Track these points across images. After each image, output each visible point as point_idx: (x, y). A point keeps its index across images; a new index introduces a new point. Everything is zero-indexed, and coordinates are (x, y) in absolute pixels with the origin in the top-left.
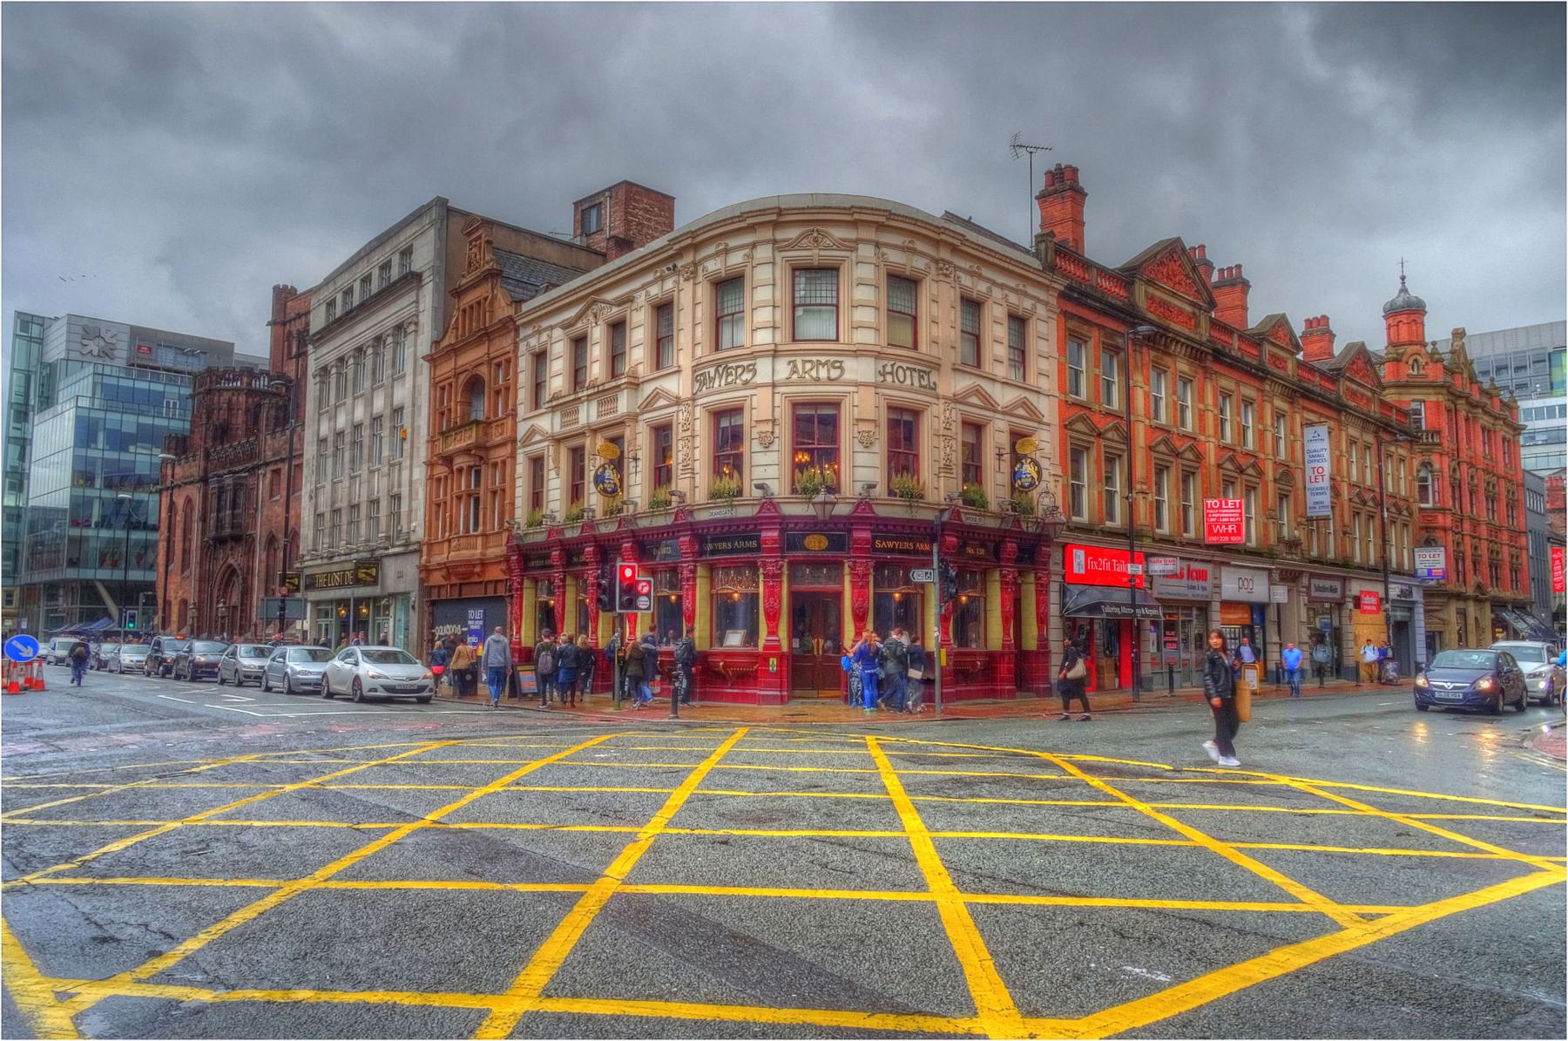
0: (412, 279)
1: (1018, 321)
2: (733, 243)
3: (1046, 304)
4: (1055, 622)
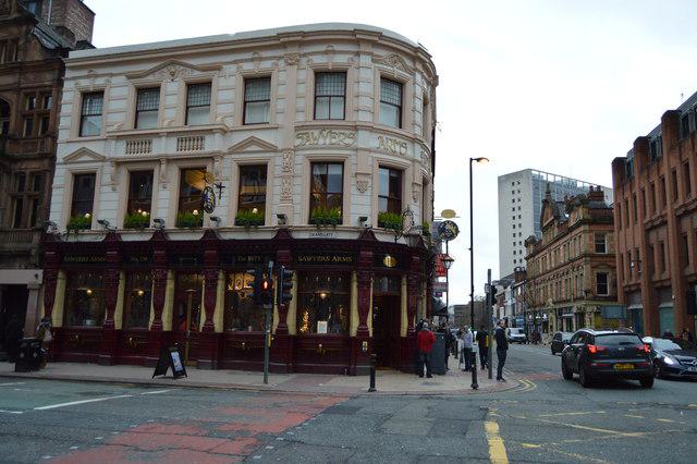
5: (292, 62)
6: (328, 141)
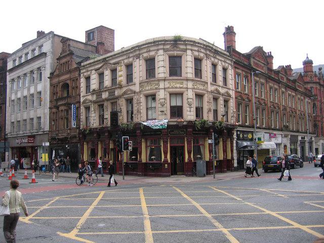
0: (43, 55)
1: (225, 70)
2: (151, 49)
3: (231, 65)
4: (235, 151)
5: (138, 57)
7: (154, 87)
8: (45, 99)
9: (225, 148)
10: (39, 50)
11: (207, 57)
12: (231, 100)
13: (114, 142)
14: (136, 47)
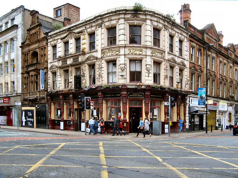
0: (15, 27)
1: (181, 42)
2: (113, 18)
3: (187, 38)
4: (187, 115)
5: (100, 26)
6: (110, 54)
7: (114, 53)
8: (18, 65)
9: (178, 112)
10: (12, 23)
11: (165, 27)
12: (186, 70)
13: (78, 102)
14: (99, 16)
